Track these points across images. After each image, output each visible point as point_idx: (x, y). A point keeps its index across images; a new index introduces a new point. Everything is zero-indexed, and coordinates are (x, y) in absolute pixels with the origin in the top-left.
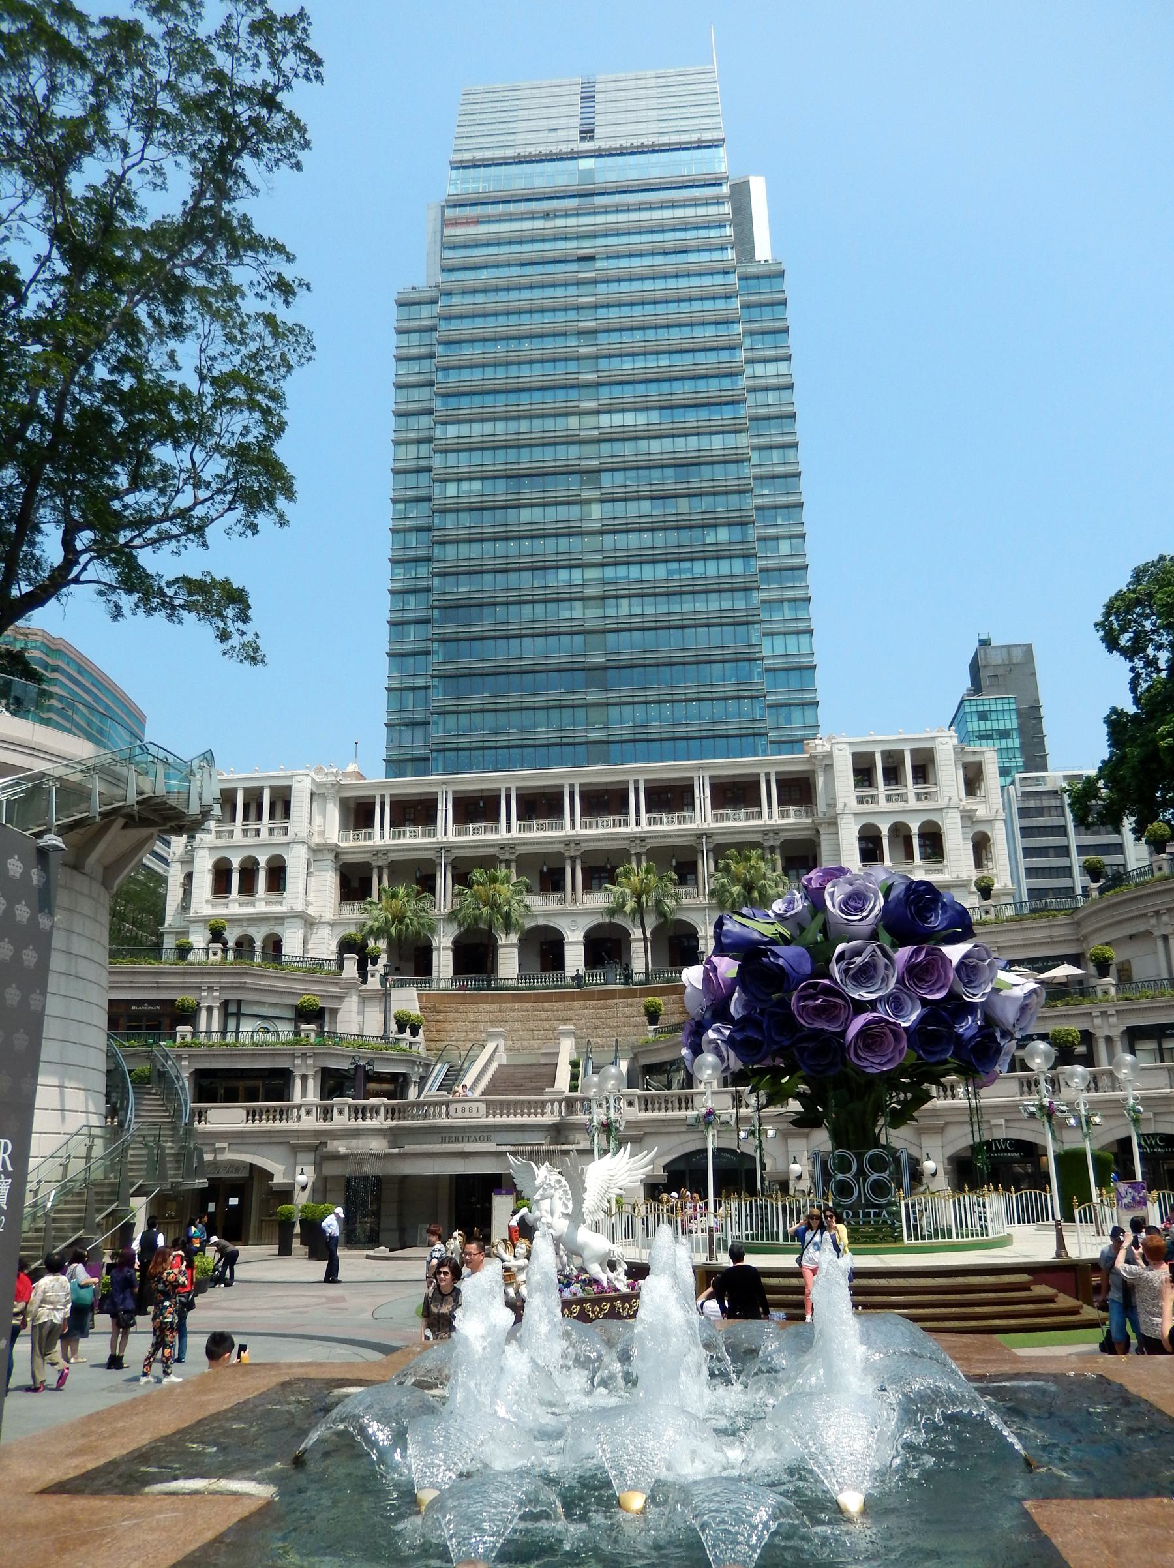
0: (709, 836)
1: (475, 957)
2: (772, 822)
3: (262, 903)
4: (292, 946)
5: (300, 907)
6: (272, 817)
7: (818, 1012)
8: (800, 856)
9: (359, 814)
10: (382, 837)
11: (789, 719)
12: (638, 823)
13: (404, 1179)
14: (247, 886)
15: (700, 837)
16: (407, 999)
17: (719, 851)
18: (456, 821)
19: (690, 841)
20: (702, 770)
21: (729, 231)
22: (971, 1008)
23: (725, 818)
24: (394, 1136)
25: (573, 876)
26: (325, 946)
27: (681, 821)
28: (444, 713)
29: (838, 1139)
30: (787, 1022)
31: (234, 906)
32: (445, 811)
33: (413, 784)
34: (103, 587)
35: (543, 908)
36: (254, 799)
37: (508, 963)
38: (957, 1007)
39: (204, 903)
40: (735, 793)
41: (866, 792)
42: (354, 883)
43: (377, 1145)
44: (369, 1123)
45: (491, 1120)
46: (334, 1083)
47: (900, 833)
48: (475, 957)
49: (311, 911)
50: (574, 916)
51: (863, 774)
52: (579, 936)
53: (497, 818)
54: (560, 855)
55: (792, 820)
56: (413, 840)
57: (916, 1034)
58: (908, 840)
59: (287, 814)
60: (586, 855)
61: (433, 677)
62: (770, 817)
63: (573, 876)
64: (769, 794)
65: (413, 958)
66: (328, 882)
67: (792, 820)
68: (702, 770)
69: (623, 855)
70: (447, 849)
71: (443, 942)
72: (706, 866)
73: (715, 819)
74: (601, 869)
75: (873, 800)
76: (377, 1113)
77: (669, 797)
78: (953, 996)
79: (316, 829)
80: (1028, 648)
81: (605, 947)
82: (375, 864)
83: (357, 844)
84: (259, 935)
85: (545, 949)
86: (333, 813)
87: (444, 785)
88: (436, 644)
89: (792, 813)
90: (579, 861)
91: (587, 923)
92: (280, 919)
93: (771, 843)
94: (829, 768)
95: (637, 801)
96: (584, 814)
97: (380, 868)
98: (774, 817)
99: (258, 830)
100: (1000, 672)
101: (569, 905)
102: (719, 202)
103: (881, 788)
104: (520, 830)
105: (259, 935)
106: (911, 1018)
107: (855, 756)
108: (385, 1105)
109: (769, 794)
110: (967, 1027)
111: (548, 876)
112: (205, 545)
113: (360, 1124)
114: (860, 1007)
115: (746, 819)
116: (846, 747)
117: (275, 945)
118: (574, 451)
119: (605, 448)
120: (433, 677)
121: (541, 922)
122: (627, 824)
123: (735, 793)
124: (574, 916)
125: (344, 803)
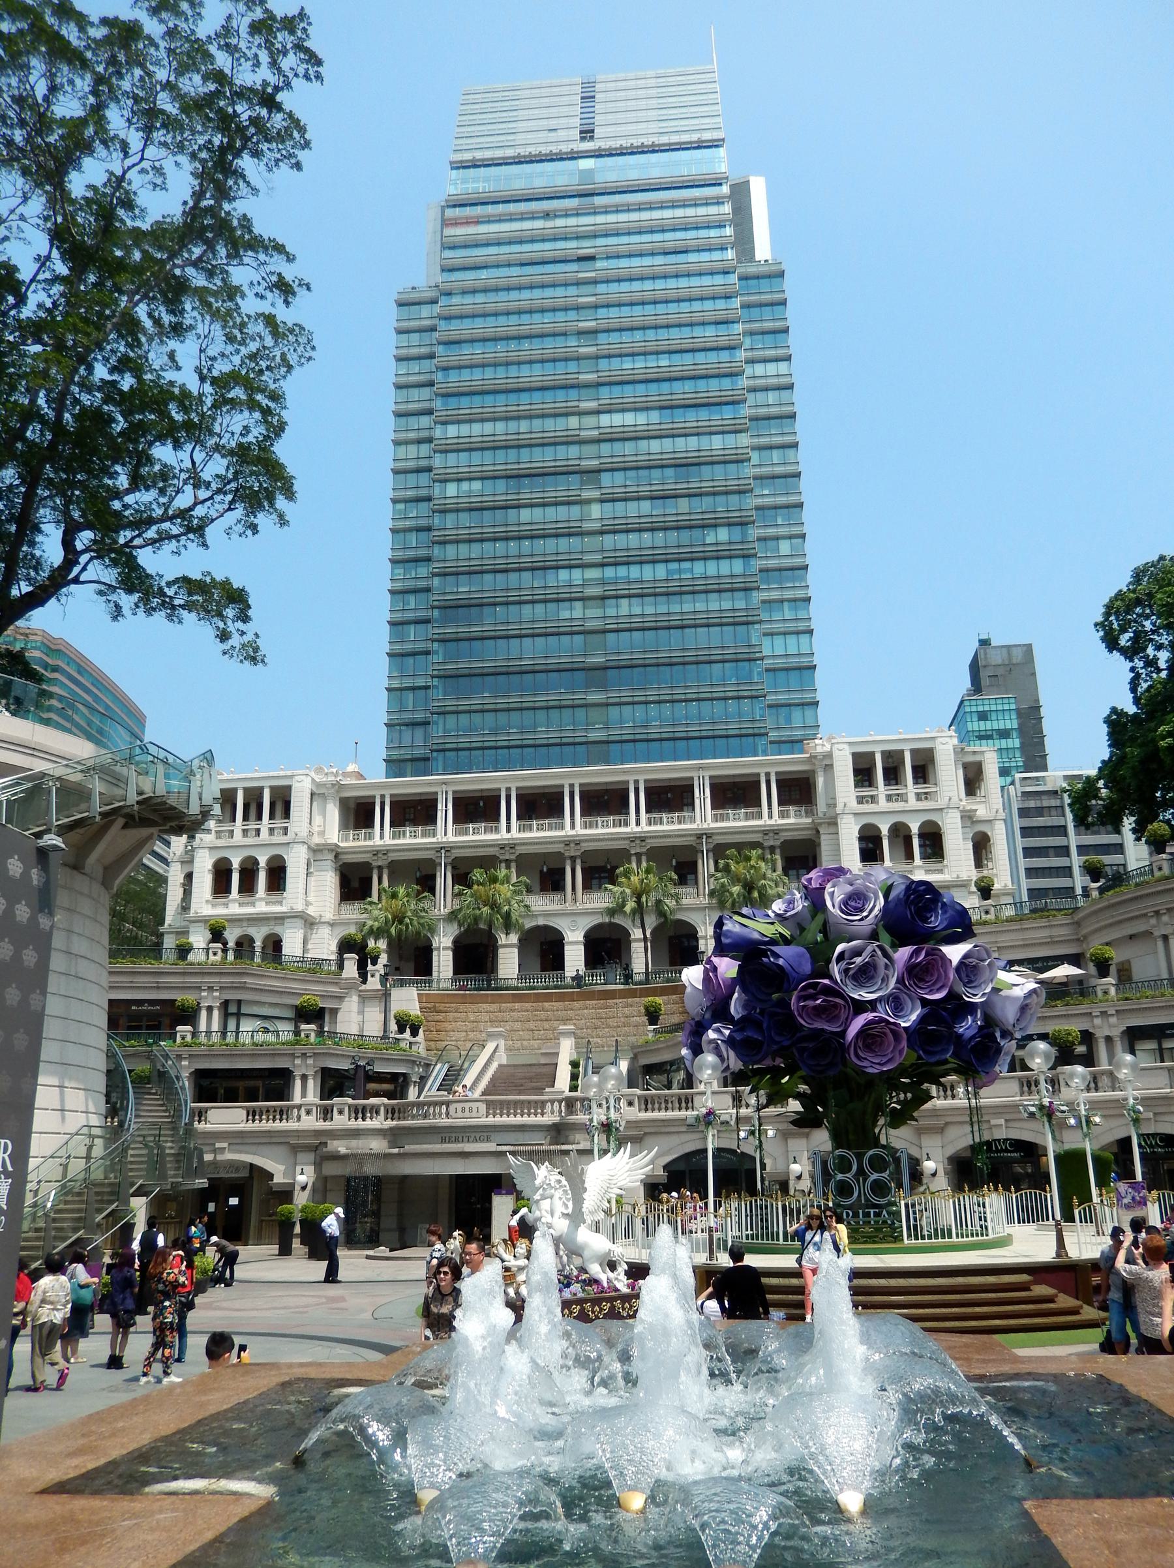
0: (709, 836)
1: (475, 957)
2: (772, 822)
3: (262, 903)
4: (292, 946)
5: (300, 907)
6: (272, 817)
7: (818, 1012)
8: (800, 856)
9: (359, 814)
10: (382, 837)
11: (789, 719)
12: (638, 823)
13: (404, 1179)
14: (247, 886)
15: (700, 837)
16: (407, 999)
17: (719, 851)
18: (456, 821)
19: (690, 841)
20: (702, 770)
21: (729, 231)
22: (971, 1008)
23: (725, 818)
24: (394, 1136)
25: (573, 876)
26: (325, 946)
27: (681, 821)
28: (444, 713)
29: (838, 1139)
30: (787, 1022)
31: (234, 906)
32: (445, 811)
33: (413, 784)
34: (103, 587)
35: (543, 908)
36: (254, 799)
37: (508, 963)
38: (957, 1007)
39: (204, 903)
40: (735, 793)
41: (866, 792)
42: (354, 883)
43: (377, 1145)
44: (369, 1123)
45: (491, 1120)
46: (334, 1083)
47: (900, 833)
48: (475, 957)
49: (311, 911)
50: (574, 916)
51: (863, 774)
52: (579, 936)
53: (497, 818)
54: (560, 855)
55: (792, 820)
56: (413, 840)
57: (916, 1034)
58: (908, 840)
59: (287, 814)
60: (586, 855)
61: (433, 677)
62: (770, 817)
63: (573, 876)
64: (769, 794)
65: (413, 958)
66: (328, 882)
67: (792, 820)
68: (702, 770)
69: (623, 855)
70: (447, 849)
71: (443, 942)
72: (706, 866)
73: (715, 819)
74: (601, 869)
75: (873, 800)
76: (377, 1113)
77: (669, 797)
78: (953, 996)
79: (316, 829)
80: (1028, 648)
81: (605, 947)
82: (375, 864)
83: (357, 844)
84: (259, 935)
85: (545, 949)
86: (333, 813)
87: (444, 785)
88: (436, 644)
89: (792, 813)
90: (579, 861)
91: (587, 923)
92: (280, 919)
93: (771, 843)
94: (829, 768)
95: (637, 801)
96: (584, 814)
97: (380, 868)
98: (774, 817)
99: (258, 830)
100: (1000, 672)
101: (569, 905)
102: (719, 202)
103: (881, 788)
104: (520, 830)
105: (259, 935)
106: (911, 1018)
107: (855, 756)
108: (385, 1105)
109: (769, 794)
110: (967, 1027)
111: (548, 876)
112: (205, 545)
113: (360, 1124)
114: (860, 1007)
115: (746, 819)
116: (846, 747)
117: (275, 945)
118: (574, 451)
119: (605, 448)
120: (433, 677)
121: (541, 922)
122: (627, 824)
123: (735, 793)
124: (574, 916)
125: (344, 803)
